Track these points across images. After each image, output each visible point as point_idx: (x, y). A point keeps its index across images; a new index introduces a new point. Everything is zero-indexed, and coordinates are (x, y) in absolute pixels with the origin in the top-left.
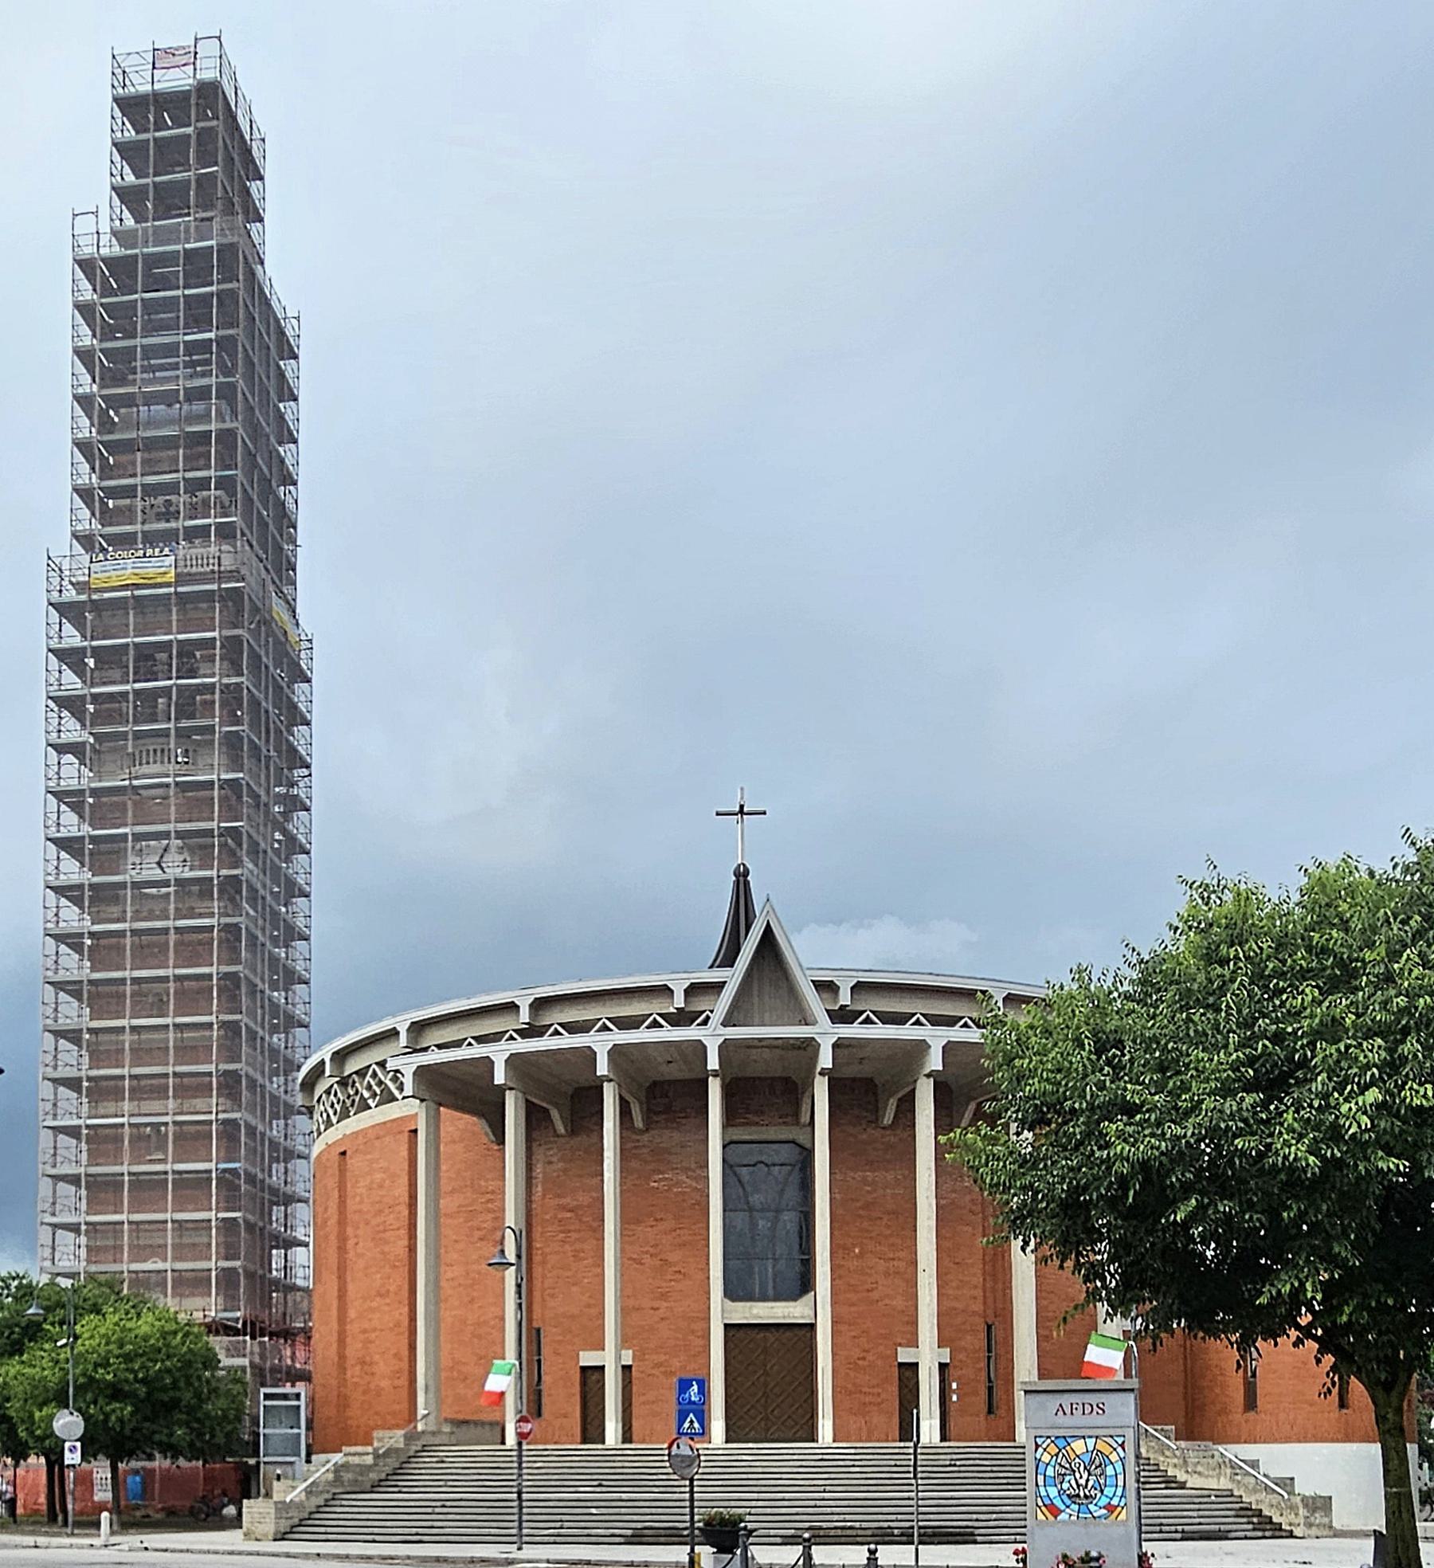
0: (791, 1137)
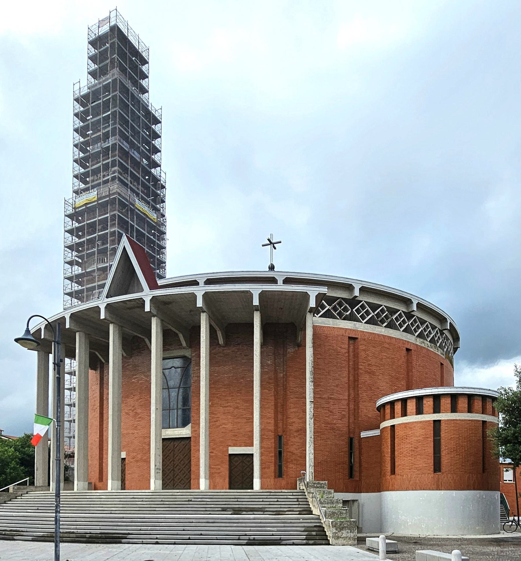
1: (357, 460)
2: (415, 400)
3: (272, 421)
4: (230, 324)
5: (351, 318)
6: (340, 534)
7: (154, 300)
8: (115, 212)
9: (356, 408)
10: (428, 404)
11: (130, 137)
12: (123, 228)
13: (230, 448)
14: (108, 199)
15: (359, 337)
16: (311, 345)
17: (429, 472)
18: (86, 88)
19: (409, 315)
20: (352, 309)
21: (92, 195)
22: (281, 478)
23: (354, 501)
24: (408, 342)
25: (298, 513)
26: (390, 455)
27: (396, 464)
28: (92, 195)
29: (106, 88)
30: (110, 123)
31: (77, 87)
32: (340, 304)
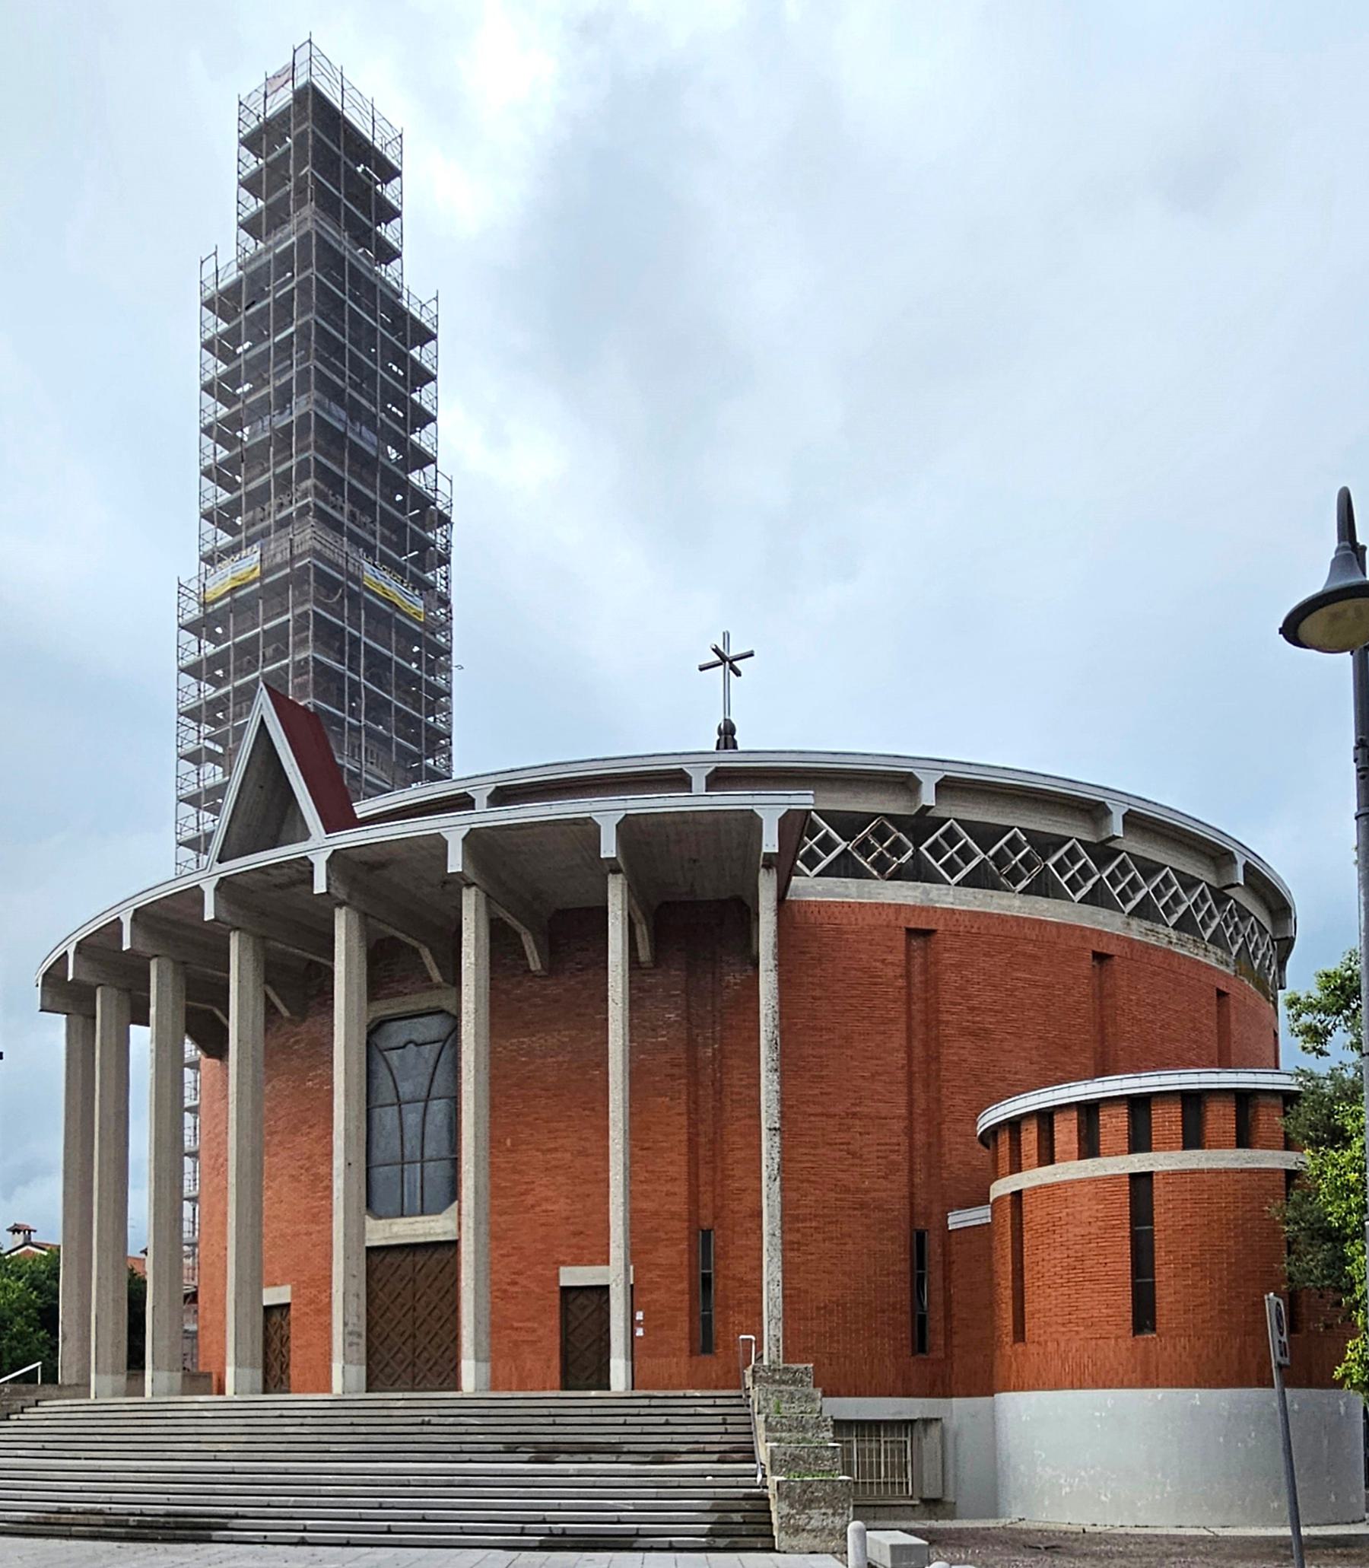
0: (434, 1004)
1: (938, 1298)
2: (1075, 1114)
3: (681, 1189)
4: (559, 912)
5: (917, 872)
6: (802, 1520)
7: (336, 859)
8: (307, 606)
9: (933, 1140)
10: (1114, 1124)
11: (349, 390)
12: (332, 648)
13: (563, 1269)
14: (288, 570)
15: (941, 928)
16: (772, 963)
17: (1120, 1332)
18: (234, 266)
19: (1103, 852)
20: (917, 844)
21: (249, 563)
22: (708, 1356)
23: (927, 1422)
24: (1100, 933)
25: (715, 1457)
26: (1010, 1284)
27: (1028, 1308)
28: (249, 563)
29: (284, 261)
30: (295, 356)
31: (209, 269)
32: (881, 834)
